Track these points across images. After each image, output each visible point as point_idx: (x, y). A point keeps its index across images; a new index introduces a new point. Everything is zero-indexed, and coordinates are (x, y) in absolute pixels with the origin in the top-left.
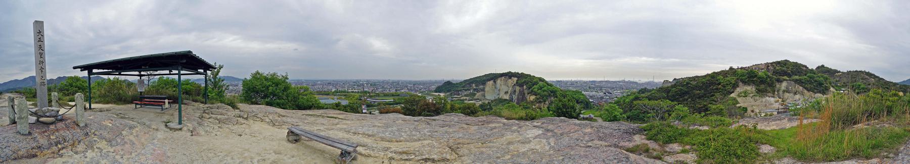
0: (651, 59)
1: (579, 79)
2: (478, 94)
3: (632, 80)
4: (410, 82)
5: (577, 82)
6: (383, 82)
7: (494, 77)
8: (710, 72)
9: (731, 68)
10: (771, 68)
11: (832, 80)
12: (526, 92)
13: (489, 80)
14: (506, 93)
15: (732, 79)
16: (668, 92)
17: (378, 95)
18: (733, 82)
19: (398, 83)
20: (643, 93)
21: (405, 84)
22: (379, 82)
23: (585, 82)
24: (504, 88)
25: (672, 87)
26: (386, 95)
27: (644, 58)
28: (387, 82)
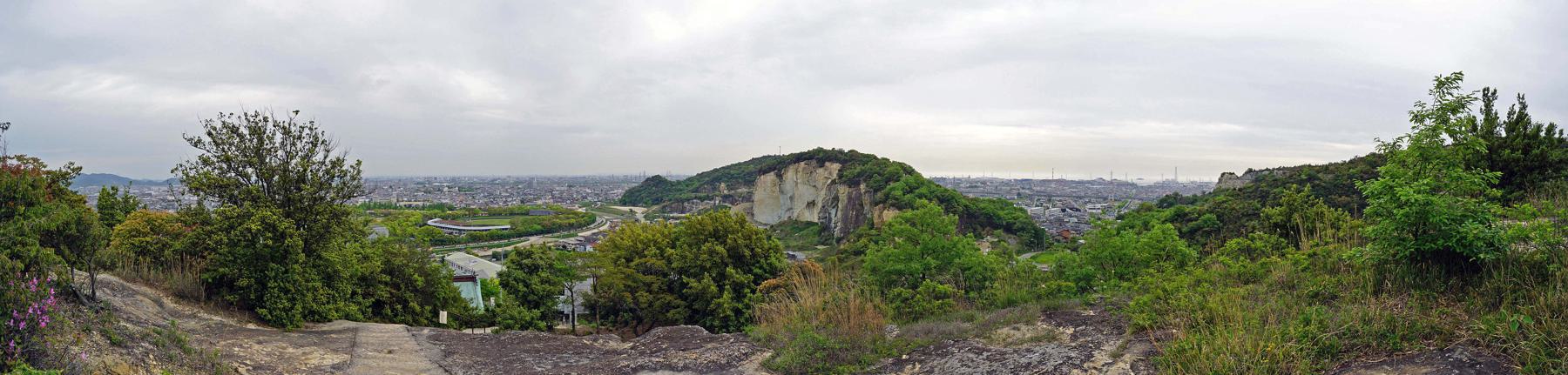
4: (560, 181)
6: (493, 182)
13: (765, 172)
14: (811, 204)
19: (529, 183)
21: (546, 186)
24: (806, 193)
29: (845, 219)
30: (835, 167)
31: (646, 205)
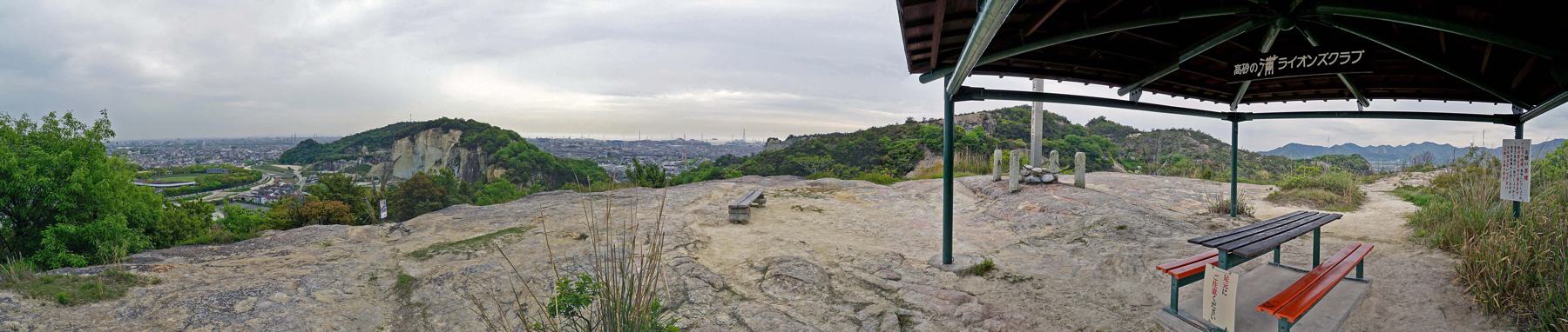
0: (737, 94)
1: (586, 136)
2: (375, 168)
3: (698, 138)
4: (224, 143)
5: (581, 143)
6: (166, 144)
7: (410, 130)
8: (865, 128)
9: (910, 121)
10: (991, 121)
11: (1120, 148)
12: (482, 160)
13: (401, 137)
14: (439, 162)
15: (911, 143)
16: (779, 162)
17: (160, 173)
18: (913, 148)
20: (726, 165)
21: (214, 148)
22: (157, 144)
23: (600, 144)
24: (434, 153)
25: (787, 151)
26: (177, 172)
27: (723, 93)
28: (176, 145)
29: (466, 175)
31: (301, 163)
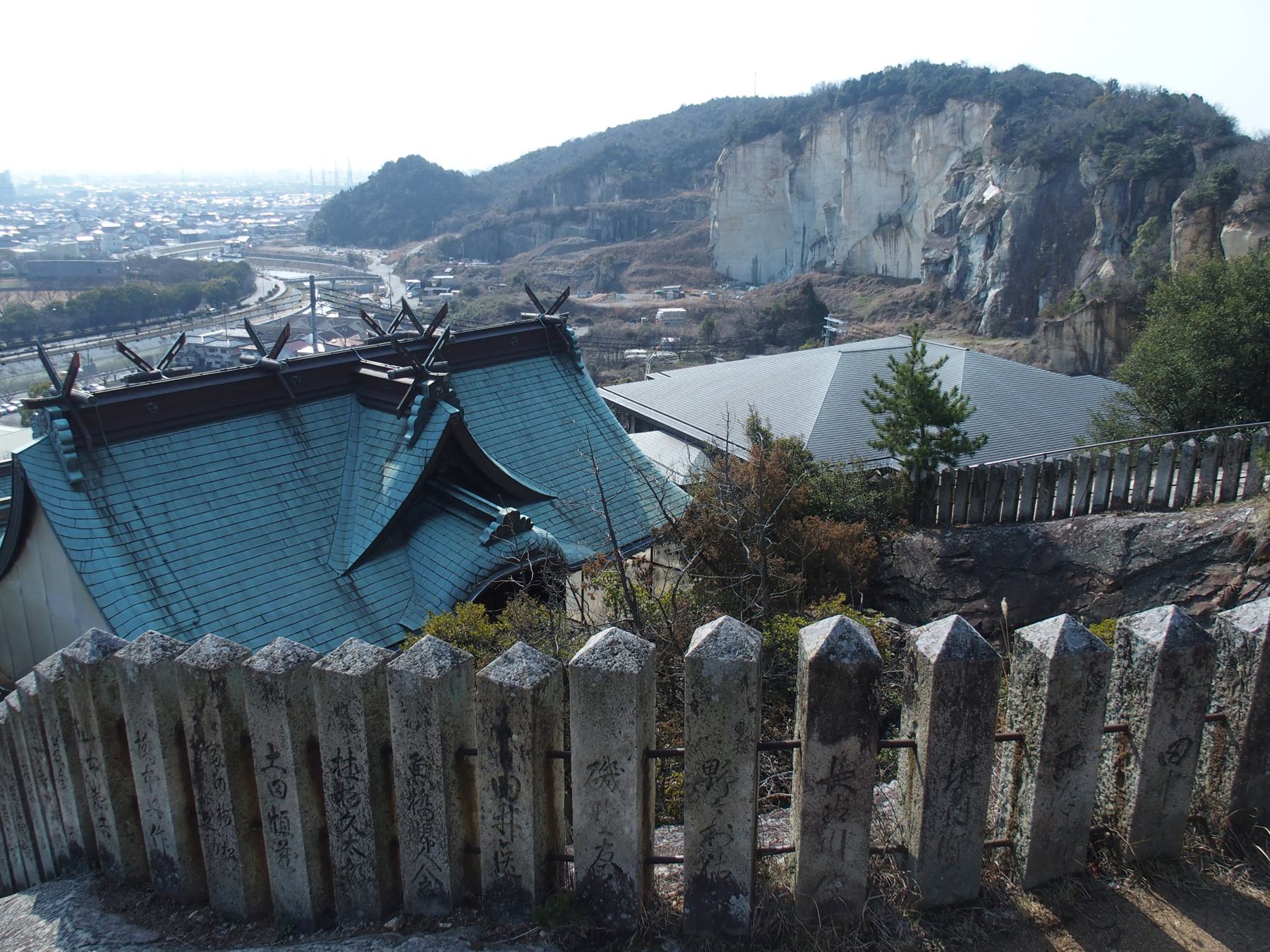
14: (891, 226)
24: (874, 192)
30: (980, 125)
